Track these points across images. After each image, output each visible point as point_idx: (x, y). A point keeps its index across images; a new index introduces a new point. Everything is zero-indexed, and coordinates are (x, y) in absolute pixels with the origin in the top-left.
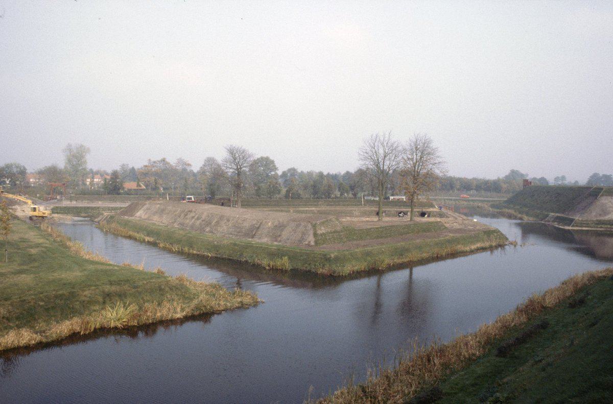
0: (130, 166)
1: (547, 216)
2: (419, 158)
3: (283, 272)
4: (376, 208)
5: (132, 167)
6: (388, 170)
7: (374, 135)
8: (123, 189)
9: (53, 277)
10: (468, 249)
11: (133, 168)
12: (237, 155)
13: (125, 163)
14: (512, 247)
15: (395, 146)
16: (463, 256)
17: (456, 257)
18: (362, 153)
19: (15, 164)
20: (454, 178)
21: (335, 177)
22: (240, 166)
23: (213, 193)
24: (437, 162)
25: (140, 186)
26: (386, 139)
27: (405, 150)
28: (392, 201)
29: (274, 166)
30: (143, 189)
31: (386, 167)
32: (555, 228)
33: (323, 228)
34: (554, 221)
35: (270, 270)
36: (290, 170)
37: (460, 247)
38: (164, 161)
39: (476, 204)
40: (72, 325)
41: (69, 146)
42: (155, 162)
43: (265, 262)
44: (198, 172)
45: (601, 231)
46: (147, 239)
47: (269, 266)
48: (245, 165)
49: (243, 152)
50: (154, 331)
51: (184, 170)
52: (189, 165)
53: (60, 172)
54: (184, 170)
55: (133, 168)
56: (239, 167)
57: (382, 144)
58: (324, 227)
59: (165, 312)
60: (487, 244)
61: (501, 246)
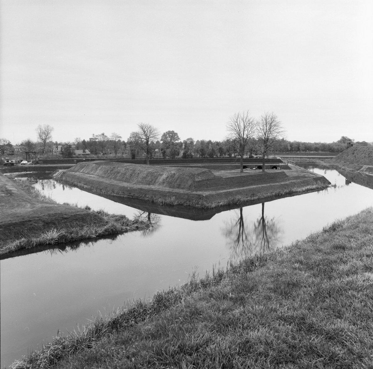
0: (82, 140)
1: (362, 167)
2: (268, 128)
3: (171, 205)
4: (239, 163)
5: (83, 140)
6: (246, 137)
7: (237, 114)
8: (75, 154)
9: (11, 212)
10: (299, 190)
11: (84, 140)
12: (146, 130)
13: (78, 137)
14: (333, 188)
15: (251, 120)
16: (304, 194)
17: (293, 196)
18: (229, 126)
19: (3, 139)
20: (301, 143)
21: (218, 144)
22: (148, 137)
23: (133, 156)
24: (280, 131)
25: (85, 152)
26: (245, 116)
27: (258, 123)
28: (254, 159)
29: (178, 137)
30: (88, 154)
31: (245, 137)
32: (367, 175)
33: (200, 177)
34: (366, 171)
35: (162, 205)
36: (188, 139)
37: (294, 190)
38: (103, 135)
39: (210, 163)
40: (20, 243)
41: (48, 126)
42: (97, 136)
43: (310, 191)
44: (271, 139)
45: (231, 188)
46: (85, 186)
47: (162, 203)
48: (151, 136)
49: (150, 127)
50: (77, 246)
51: (119, 141)
52: (120, 137)
53: (35, 145)
54: (108, 141)
55: (84, 140)
56: (147, 137)
57: (243, 119)
58: (201, 176)
59: (83, 233)
60: (314, 187)
61: (324, 188)
